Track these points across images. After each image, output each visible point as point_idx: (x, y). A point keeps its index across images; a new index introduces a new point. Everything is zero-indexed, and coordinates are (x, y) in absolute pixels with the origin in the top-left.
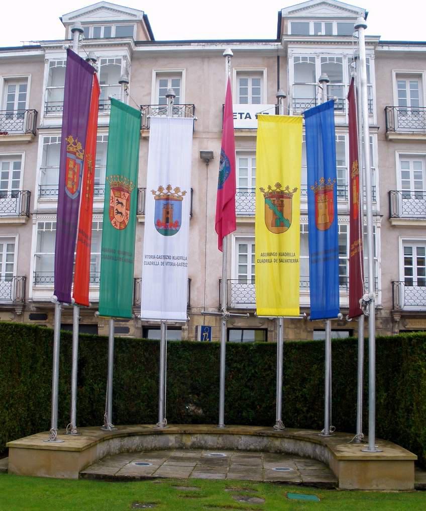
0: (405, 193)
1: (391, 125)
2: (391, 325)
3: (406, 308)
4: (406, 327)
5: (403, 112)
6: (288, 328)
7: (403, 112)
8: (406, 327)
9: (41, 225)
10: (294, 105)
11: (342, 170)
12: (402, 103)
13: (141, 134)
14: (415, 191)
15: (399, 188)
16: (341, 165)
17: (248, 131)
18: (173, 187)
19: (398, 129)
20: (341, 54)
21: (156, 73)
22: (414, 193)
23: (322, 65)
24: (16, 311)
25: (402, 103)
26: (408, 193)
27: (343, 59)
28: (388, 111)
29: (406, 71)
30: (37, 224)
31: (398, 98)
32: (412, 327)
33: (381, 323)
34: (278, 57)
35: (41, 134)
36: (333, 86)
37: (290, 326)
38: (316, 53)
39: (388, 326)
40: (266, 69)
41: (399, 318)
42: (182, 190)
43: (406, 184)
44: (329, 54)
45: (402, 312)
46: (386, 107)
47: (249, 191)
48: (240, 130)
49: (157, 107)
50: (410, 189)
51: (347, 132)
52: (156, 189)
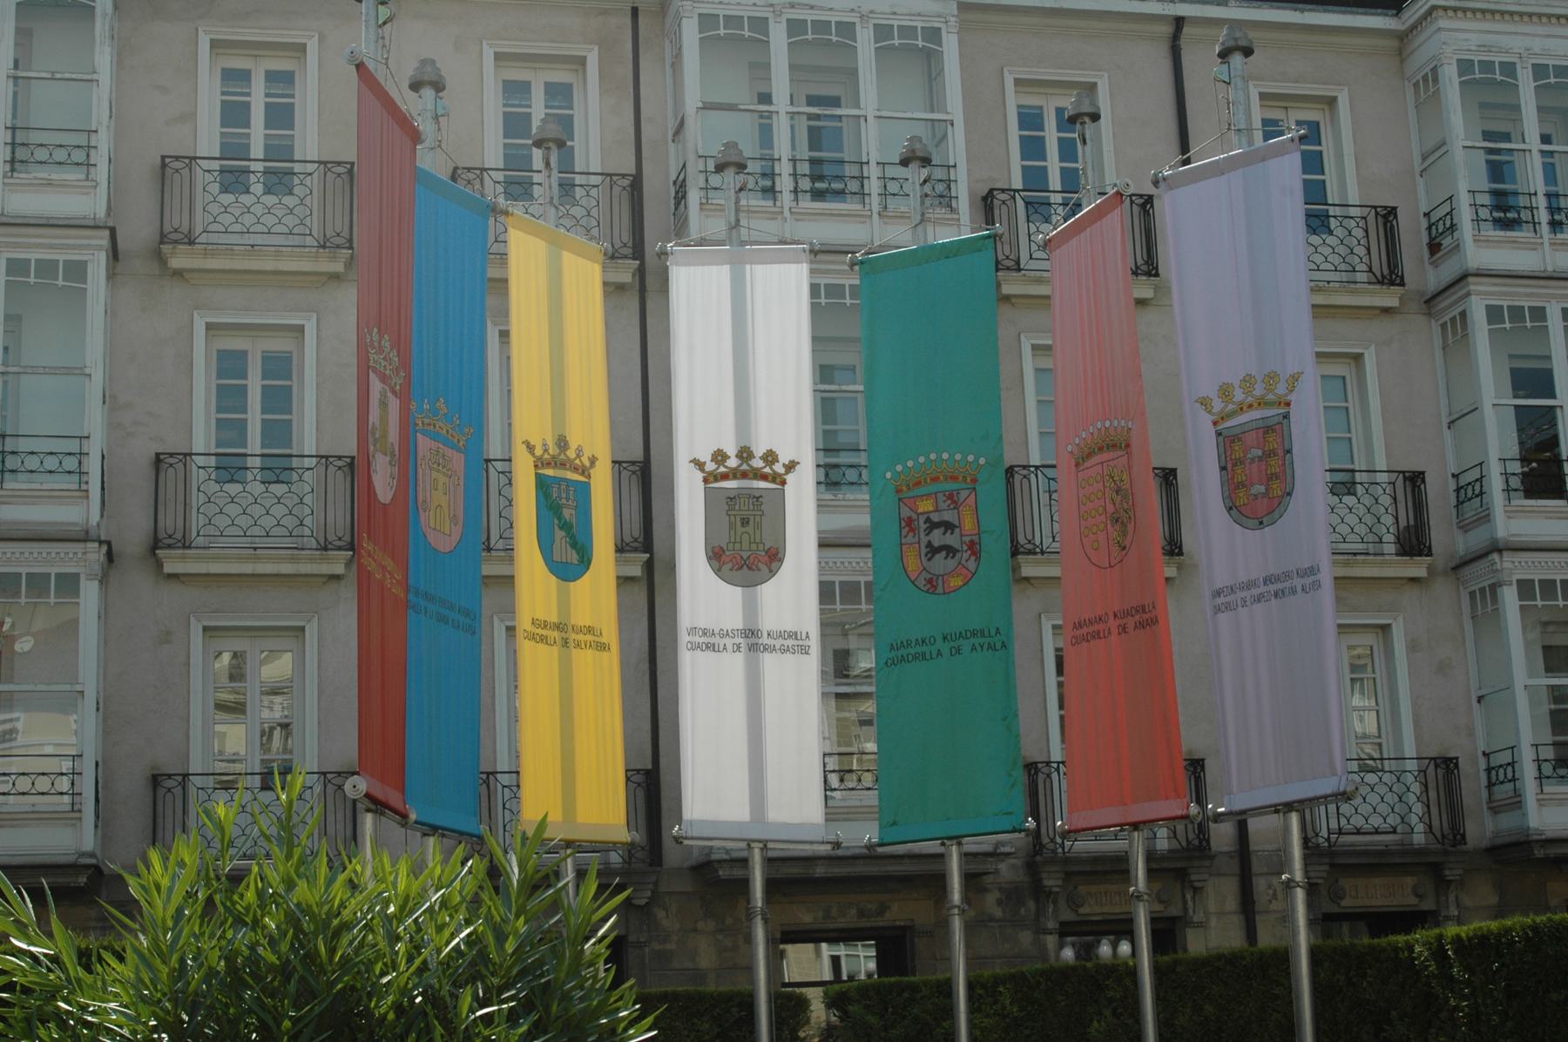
0: (271, 462)
1: (1007, 253)
2: (1032, 904)
3: (1083, 846)
4: (1081, 911)
5: (234, 180)
6: (695, 930)
7: (234, 180)
8: (1081, 911)
9: (1525, 588)
10: (702, 177)
11: (834, 399)
12: (234, 150)
13: (999, 285)
14: (262, 455)
15: (202, 439)
16: (831, 383)
17: (227, 249)
18: (759, 451)
19: (1033, 265)
20: (852, 10)
21: (211, 40)
22: (257, 462)
23: (789, 44)
24: (1193, 877)
25: (1035, 179)
26: (238, 462)
27: (771, 21)
28: (169, 171)
29: (1310, 89)
30: (1515, 582)
31: (501, 141)
32: (1098, 910)
33: (999, 902)
34: (635, 12)
35: (1479, 293)
36: (932, 120)
37: (700, 925)
38: (772, 5)
39: (1023, 911)
40: (596, 48)
41: (1059, 882)
42: (784, 458)
43: (232, 429)
44: (812, 8)
45: (1067, 860)
46: (991, 191)
47: (251, 462)
48: (101, 238)
49: (216, 165)
50: (246, 447)
51: (99, 248)
52: (705, 457)
